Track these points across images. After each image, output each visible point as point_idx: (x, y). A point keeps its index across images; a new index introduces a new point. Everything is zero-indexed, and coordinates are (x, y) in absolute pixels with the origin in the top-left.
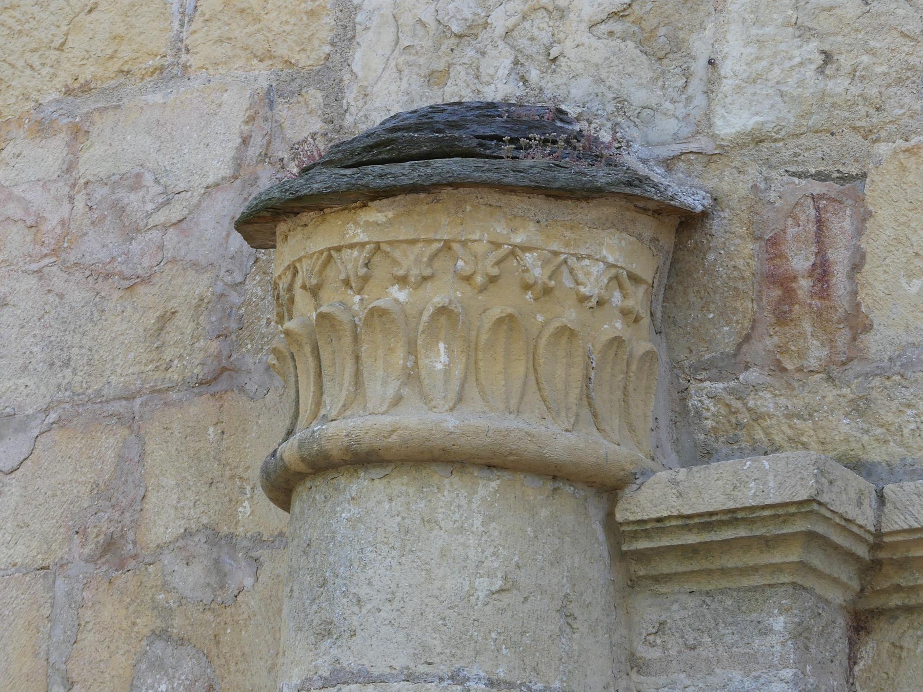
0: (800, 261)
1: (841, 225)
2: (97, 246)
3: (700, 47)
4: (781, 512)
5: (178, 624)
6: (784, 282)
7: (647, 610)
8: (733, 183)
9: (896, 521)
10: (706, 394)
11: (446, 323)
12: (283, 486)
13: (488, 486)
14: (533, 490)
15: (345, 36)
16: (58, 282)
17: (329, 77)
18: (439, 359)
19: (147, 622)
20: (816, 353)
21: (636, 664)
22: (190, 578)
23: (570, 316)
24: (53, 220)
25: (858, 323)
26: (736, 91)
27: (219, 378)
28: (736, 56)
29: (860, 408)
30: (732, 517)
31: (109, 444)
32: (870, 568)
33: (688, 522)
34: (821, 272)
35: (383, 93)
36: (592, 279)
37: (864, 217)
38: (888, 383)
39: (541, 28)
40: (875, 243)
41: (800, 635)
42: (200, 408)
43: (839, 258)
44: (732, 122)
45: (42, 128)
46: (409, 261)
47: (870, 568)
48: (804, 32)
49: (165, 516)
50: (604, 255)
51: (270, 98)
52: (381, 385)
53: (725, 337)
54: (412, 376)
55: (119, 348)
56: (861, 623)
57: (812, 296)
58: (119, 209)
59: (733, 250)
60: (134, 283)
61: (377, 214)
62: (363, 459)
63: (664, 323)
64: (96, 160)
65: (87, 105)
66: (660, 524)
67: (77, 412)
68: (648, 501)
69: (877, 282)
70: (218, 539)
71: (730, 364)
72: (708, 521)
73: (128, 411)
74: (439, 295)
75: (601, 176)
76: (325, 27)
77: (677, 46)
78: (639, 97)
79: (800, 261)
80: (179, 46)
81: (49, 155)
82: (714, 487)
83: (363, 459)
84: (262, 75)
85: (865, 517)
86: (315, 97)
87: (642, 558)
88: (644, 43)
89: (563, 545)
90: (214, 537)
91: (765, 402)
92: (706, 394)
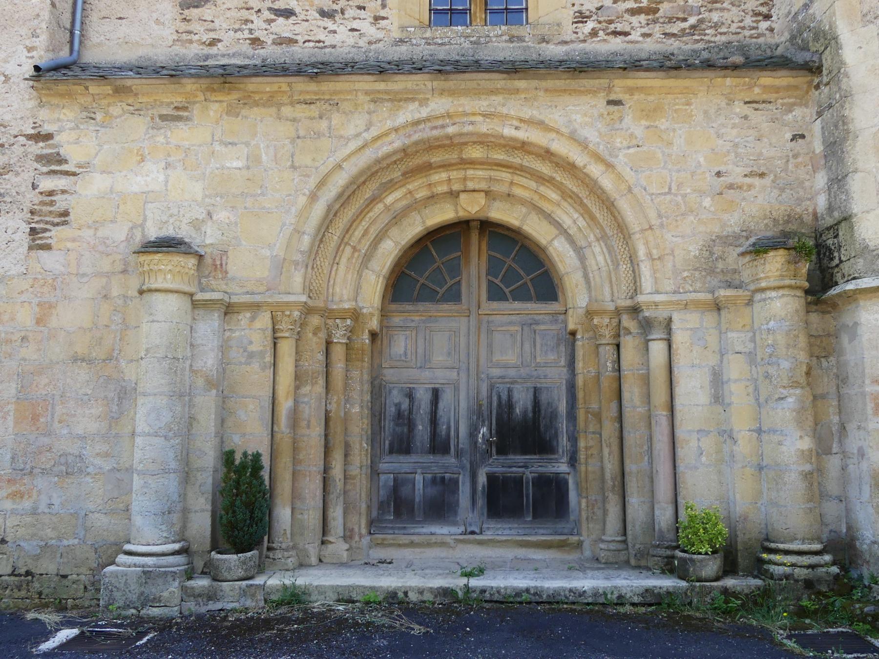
0: (218, 263)
1: (224, 258)
2: (101, 248)
3: (203, 229)
4: (218, 300)
5: (118, 309)
6: (216, 266)
7: (196, 312)
8: (209, 250)
9: (232, 301)
10: (203, 280)
11: (169, 270)
12: (141, 292)
13: (176, 295)
14: (182, 295)
15: (145, 220)
16: (94, 253)
17: (142, 226)
18: (169, 276)
19: (112, 308)
20: (220, 276)
21: (194, 319)
22: (120, 302)
23: (187, 270)
24: (92, 243)
25: (226, 272)
26: (208, 238)
27: (124, 271)
28: (209, 232)
29: (226, 284)
30: (210, 300)
31: (104, 280)
32: (228, 307)
33: (204, 300)
34: (221, 265)
35: (153, 234)
36: (190, 265)
37: (227, 258)
38: (114, 589)
39: (178, 223)
40: (229, 261)
41: (219, 316)
42: (121, 276)
43: (224, 263)
44: (208, 242)
45: (89, 227)
46: (165, 262)
47: (228, 307)
48: (220, 230)
49: (115, 293)
50: (192, 261)
51: (132, 228)
52: (160, 279)
53: (207, 273)
54: (165, 279)
55: (105, 265)
56: (226, 314)
57: (220, 268)
58: (105, 243)
59: (208, 260)
60: (108, 255)
61: (159, 255)
62: (157, 290)
63: (198, 270)
64: (100, 234)
65: (98, 225)
66: (199, 300)
67: (99, 274)
68: (196, 297)
69: (229, 267)
70: (125, 297)
71: (207, 277)
72: (207, 301)
73: (108, 275)
74: (169, 267)
75: (189, 250)
76: (142, 218)
77: (199, 229)
78: (194, 236)
79: (218, 263)
80: (115, 217)
81: (91, 232)
82: (208, 296)
83: (157, 290)
84: (130, 225)
85: (228, 300)
86: (140, 229)
87: (196, 305)
88: (194, 227)
89: (186, 303)
90: (124, 296)
91: (213, 282)
92: (203, 280)
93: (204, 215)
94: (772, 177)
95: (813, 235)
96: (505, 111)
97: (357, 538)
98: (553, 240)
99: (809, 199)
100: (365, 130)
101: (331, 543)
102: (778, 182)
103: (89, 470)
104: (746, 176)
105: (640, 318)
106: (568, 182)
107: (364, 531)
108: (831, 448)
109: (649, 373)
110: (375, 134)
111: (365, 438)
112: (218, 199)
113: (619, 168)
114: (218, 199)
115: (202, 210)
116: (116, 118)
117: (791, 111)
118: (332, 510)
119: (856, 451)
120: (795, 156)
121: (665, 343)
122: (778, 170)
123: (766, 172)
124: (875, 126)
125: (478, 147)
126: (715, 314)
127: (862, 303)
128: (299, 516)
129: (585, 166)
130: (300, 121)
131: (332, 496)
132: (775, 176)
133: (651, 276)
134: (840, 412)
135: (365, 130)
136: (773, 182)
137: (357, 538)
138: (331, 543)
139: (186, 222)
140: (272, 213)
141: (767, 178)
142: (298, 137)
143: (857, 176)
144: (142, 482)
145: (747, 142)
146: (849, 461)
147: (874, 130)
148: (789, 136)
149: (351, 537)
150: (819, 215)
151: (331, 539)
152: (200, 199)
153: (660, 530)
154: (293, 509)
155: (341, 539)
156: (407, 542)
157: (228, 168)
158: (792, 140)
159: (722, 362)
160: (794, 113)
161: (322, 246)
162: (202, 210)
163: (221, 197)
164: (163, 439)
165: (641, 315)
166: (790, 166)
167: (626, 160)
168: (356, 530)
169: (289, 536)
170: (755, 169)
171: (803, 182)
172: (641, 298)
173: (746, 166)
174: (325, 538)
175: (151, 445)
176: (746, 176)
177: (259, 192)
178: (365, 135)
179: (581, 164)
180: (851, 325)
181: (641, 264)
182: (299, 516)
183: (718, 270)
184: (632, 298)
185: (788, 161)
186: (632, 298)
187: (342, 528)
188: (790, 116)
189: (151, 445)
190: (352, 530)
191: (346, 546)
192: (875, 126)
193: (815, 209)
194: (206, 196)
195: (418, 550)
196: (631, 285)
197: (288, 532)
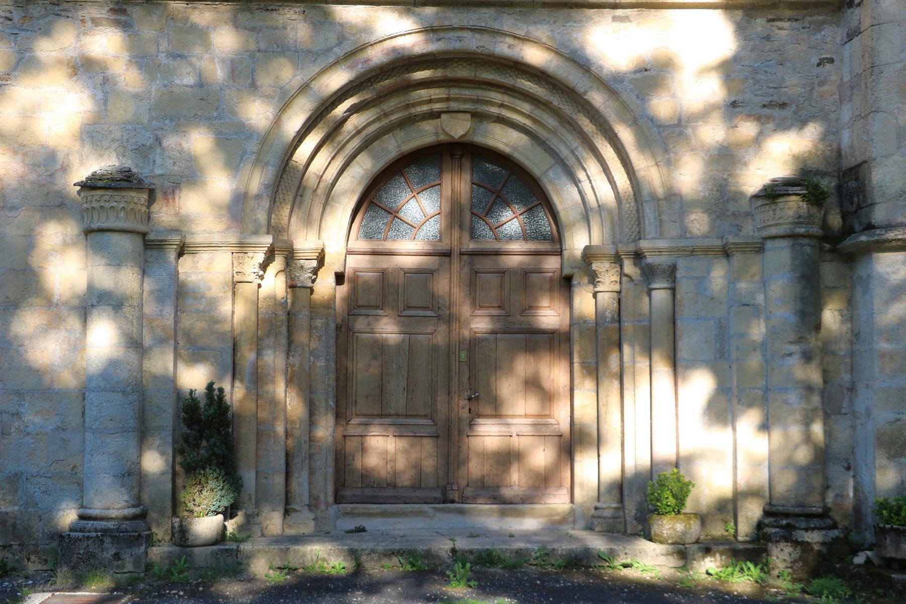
3: (151, 157)
7: (149, 253)
13: (130, 235)
46: (117, 198)
66: (153, 241)
93: (151, 141)
94: (794, 107)
95: (836, 174)
96: (497, 26)
97: (323, 507)
98: (548, 170)
99: (834, 134)
100: (337, 45)
101: (296, 511)
102: (800, 113)
103: (28, 430)
104: (764, 106)
105: (643, 264)
106: (567, 107)
107: (331, 499)
108: (840, 408)
109: (650, 326)
110: (349, 50)
111: (331, 395)
112: (167, 122)
113: (624, 96)
114: (167, 122)
115: (148, 134)
116: (38, 19)
117: (820, 31)
118: (296, 475)
119: (863, 411)
120: (822, 83)
121: (669, 292)
122: (802, 100)
123: (787, 102)
124: (901, 61)
125: (465, 64)
126: (724, 261)
127: (543, 469)
128: (264, 481)
129: (585, 92)
130: (260, 31)
131: (296, 460)
132: (797, 106)
133: (655, 218)
134: (852, 370)
135: (337, 45)
136: (795, 113)
137: (323, 507)
138: (296, 511)
139: (131, 148)
140: (230, 140)
141: (788, 109)
142: (259, 51)
143: (880, 116)
144: (99, 441)
145: (768, 66)
146: (858, 422)
147: (899, 66)
148: (815, 60)
149: (317, 506)
150: (843, 153)
151: (296, 507)
152: (146, 121)
153: (718, 567)
154: (257, 473)
155: (307, 508)
156: (379, 511)
157: (178, 85)
158: (818, 65)
159: (729, 313)
160: (823, 33)
161: (285, 176)
162: (148, 134)
163: (171, 120)
164: (121, 395)
165: (644, 262)
166: (815, 96)
167: (631, 86)
168: (322, 497)
169: (254, 501)
170: (775, 98)
171: (827, 114)
172: (644, 244)
173: (766, 95)
174: (289, 507)
175: (108, 401)
176: (764, 106)
177: (215, 115)
178: (336, 50)
179: (582, 90)
180: (864, 277)
181: (644, 204)
182: (264, 481)
183: (729, 213)
184: (634, 241)
185: (813, 89)
186: (634, 241)
187: (307, 495)
188: (818, 36)
189: (108, 401)
190: (317, 498)
191: (312, 516)
192: (901, 61)
193: (839, 145)
194: (349, 252)
195: (392, 520)
196: (635, 226)
197: (253, 497)
